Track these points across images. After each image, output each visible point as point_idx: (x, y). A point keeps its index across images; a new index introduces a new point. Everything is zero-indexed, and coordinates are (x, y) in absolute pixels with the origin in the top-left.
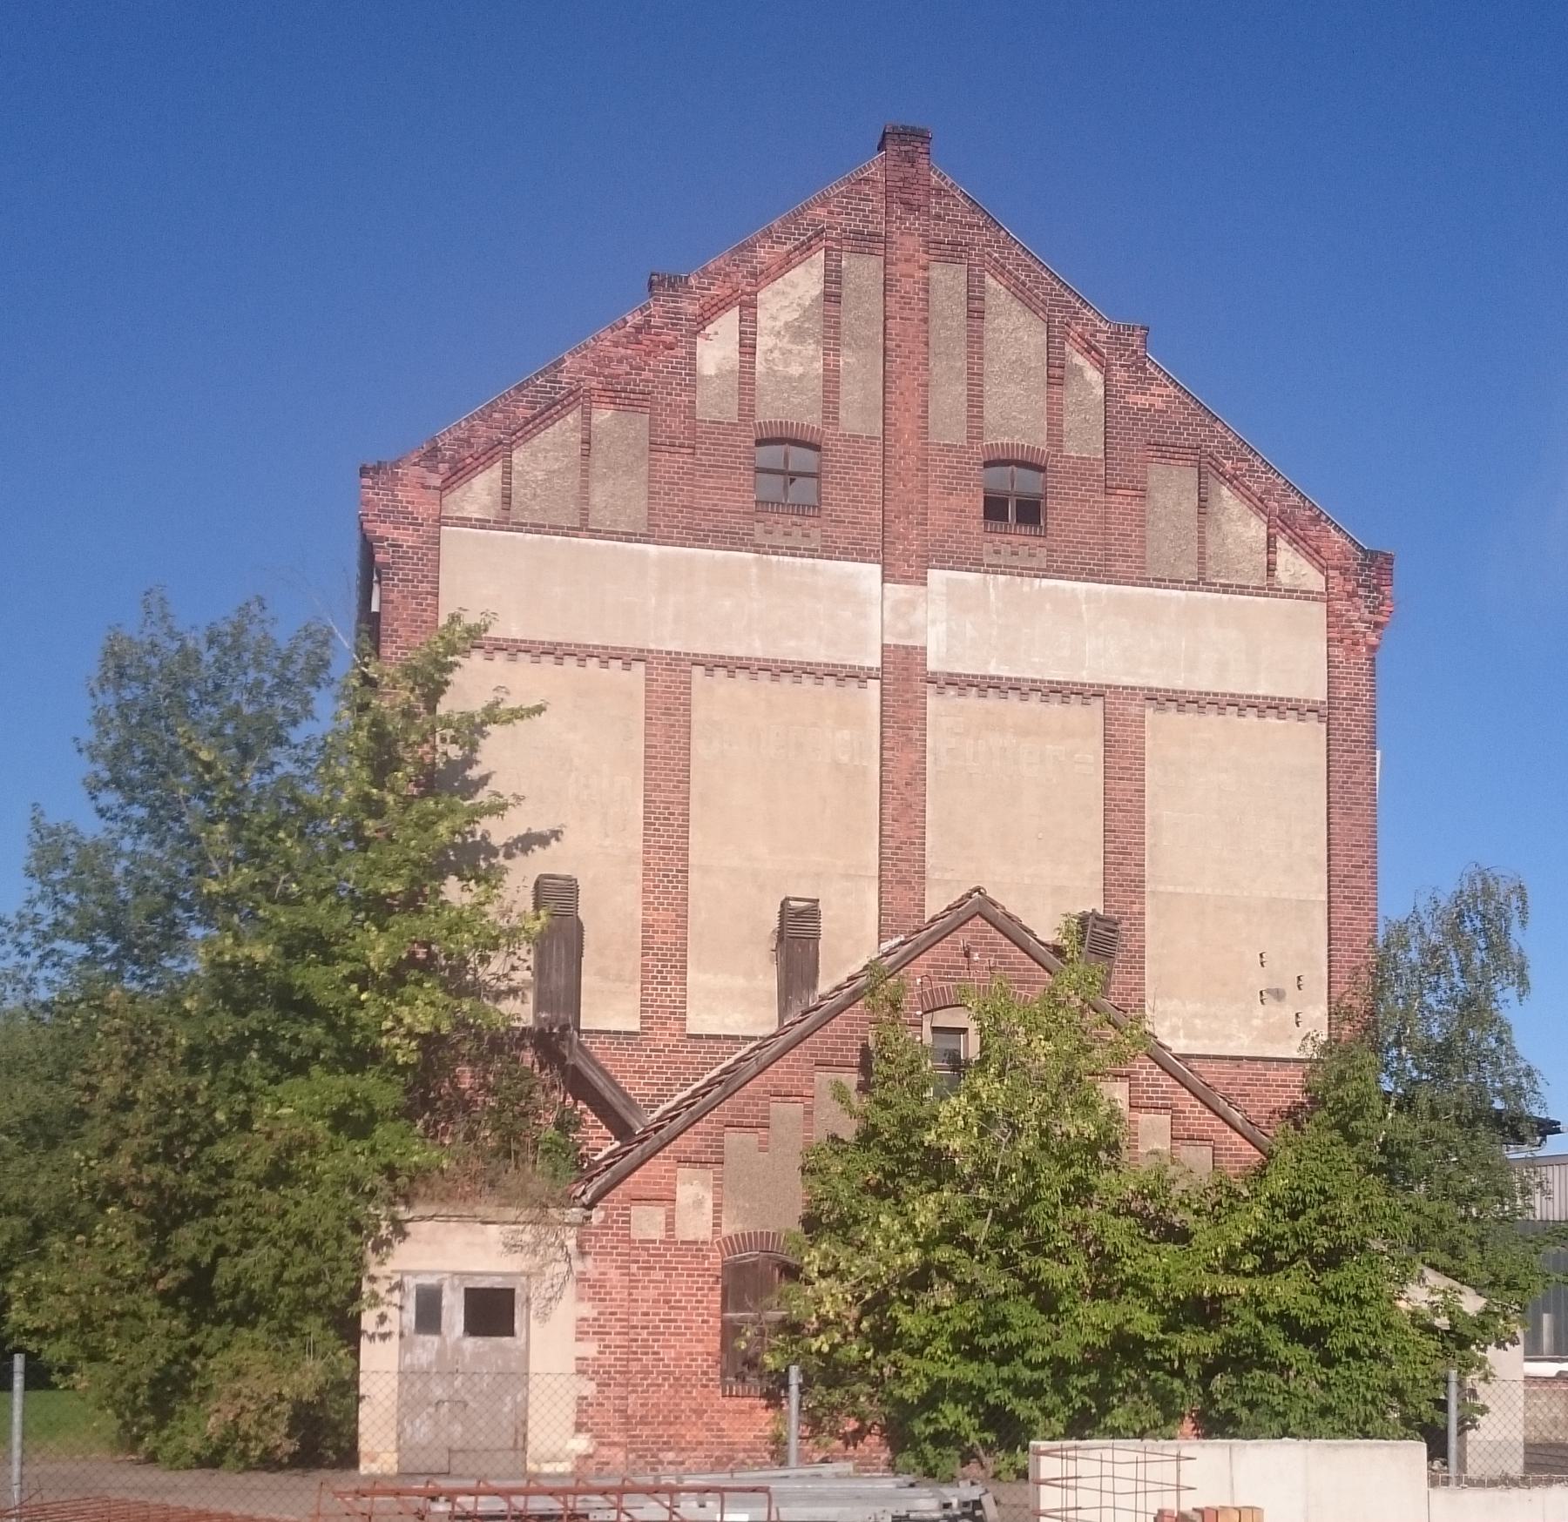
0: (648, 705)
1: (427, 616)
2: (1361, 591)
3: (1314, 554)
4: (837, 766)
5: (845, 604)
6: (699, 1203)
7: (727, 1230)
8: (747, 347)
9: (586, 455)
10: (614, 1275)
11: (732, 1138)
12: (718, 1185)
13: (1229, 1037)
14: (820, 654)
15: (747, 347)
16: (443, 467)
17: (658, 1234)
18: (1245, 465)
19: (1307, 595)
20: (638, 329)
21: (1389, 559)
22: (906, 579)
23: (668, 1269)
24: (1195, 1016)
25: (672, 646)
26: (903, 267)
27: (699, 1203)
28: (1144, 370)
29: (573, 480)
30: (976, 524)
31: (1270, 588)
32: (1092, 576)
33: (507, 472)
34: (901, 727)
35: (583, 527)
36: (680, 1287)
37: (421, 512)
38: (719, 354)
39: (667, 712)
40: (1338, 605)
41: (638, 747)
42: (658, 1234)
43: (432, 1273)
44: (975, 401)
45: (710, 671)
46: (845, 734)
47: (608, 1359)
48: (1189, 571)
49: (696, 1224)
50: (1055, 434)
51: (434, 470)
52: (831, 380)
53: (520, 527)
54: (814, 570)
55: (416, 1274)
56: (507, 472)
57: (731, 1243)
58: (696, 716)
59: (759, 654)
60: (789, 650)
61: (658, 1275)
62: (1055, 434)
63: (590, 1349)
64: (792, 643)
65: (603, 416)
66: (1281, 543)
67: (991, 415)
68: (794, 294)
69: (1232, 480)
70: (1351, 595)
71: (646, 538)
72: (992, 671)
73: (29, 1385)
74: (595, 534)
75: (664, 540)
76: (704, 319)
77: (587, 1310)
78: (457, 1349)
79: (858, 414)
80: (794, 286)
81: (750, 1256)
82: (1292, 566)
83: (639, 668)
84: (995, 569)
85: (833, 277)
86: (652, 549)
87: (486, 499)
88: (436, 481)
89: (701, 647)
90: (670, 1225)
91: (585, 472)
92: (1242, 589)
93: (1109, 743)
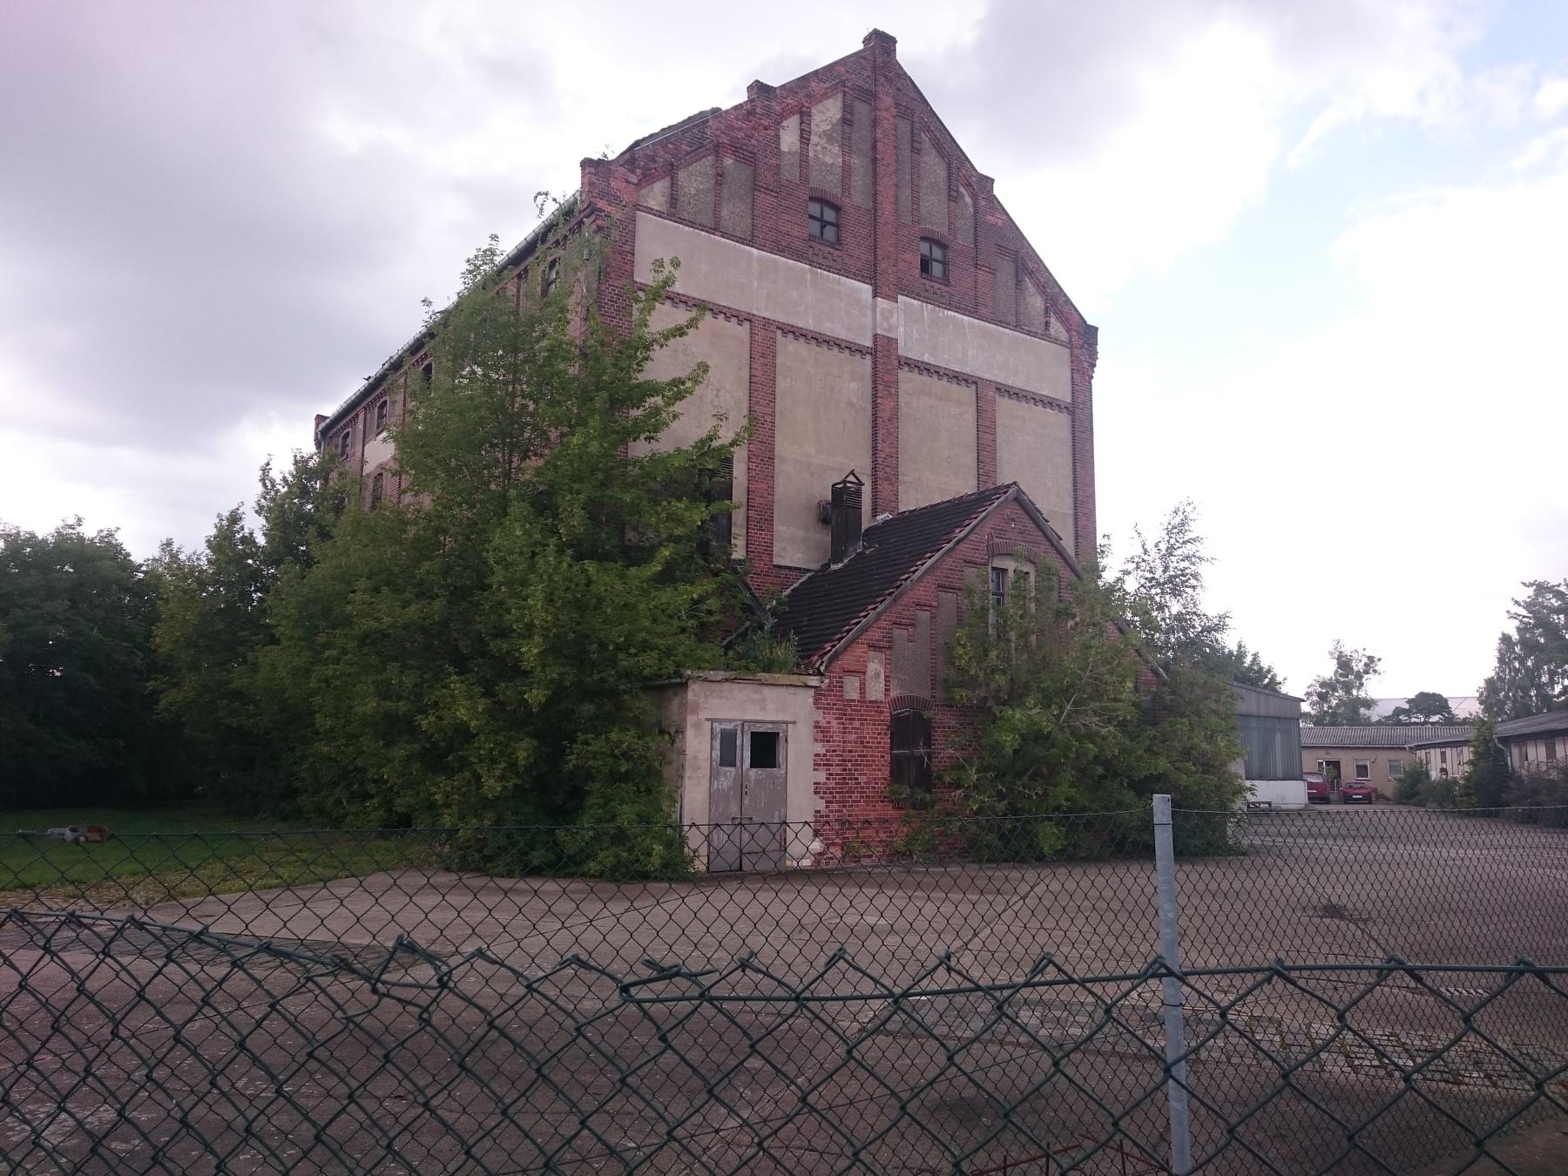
1: (627, 267)
6: (877, 675)
7: (894, 693)
9: (718, 184)
10: (834, 723)
11: (898, 632)
12: (888, 662)
14: (842, 334)
15: (805, 138)
16: (638, 171)
22: (887, 297)
25: (765, 315)
31: (1046, 336)
34: (882, 387)
35: (715, 229)
37: (626, 198)
39: (763, 356)
42: (855, 695)
43: (731, 721)
47: (832, 784)
49: (876, 691)
51: (633, 172)
52: (846, 170)
53: (681, 221)
54: (839, 282)
55: (720, 721)
56: (673, 184)
57: (896, 703)
58: (779, 360)
61: (857, 724)
63: (821, 776)
73: (1182, 853)
77: (820, 748)
79: (858, 197)
81: (905, 711)
85: (847, 109)
87: (662, 199)
89: (781, 318)
91: (718, 195)
93: (979, 411)
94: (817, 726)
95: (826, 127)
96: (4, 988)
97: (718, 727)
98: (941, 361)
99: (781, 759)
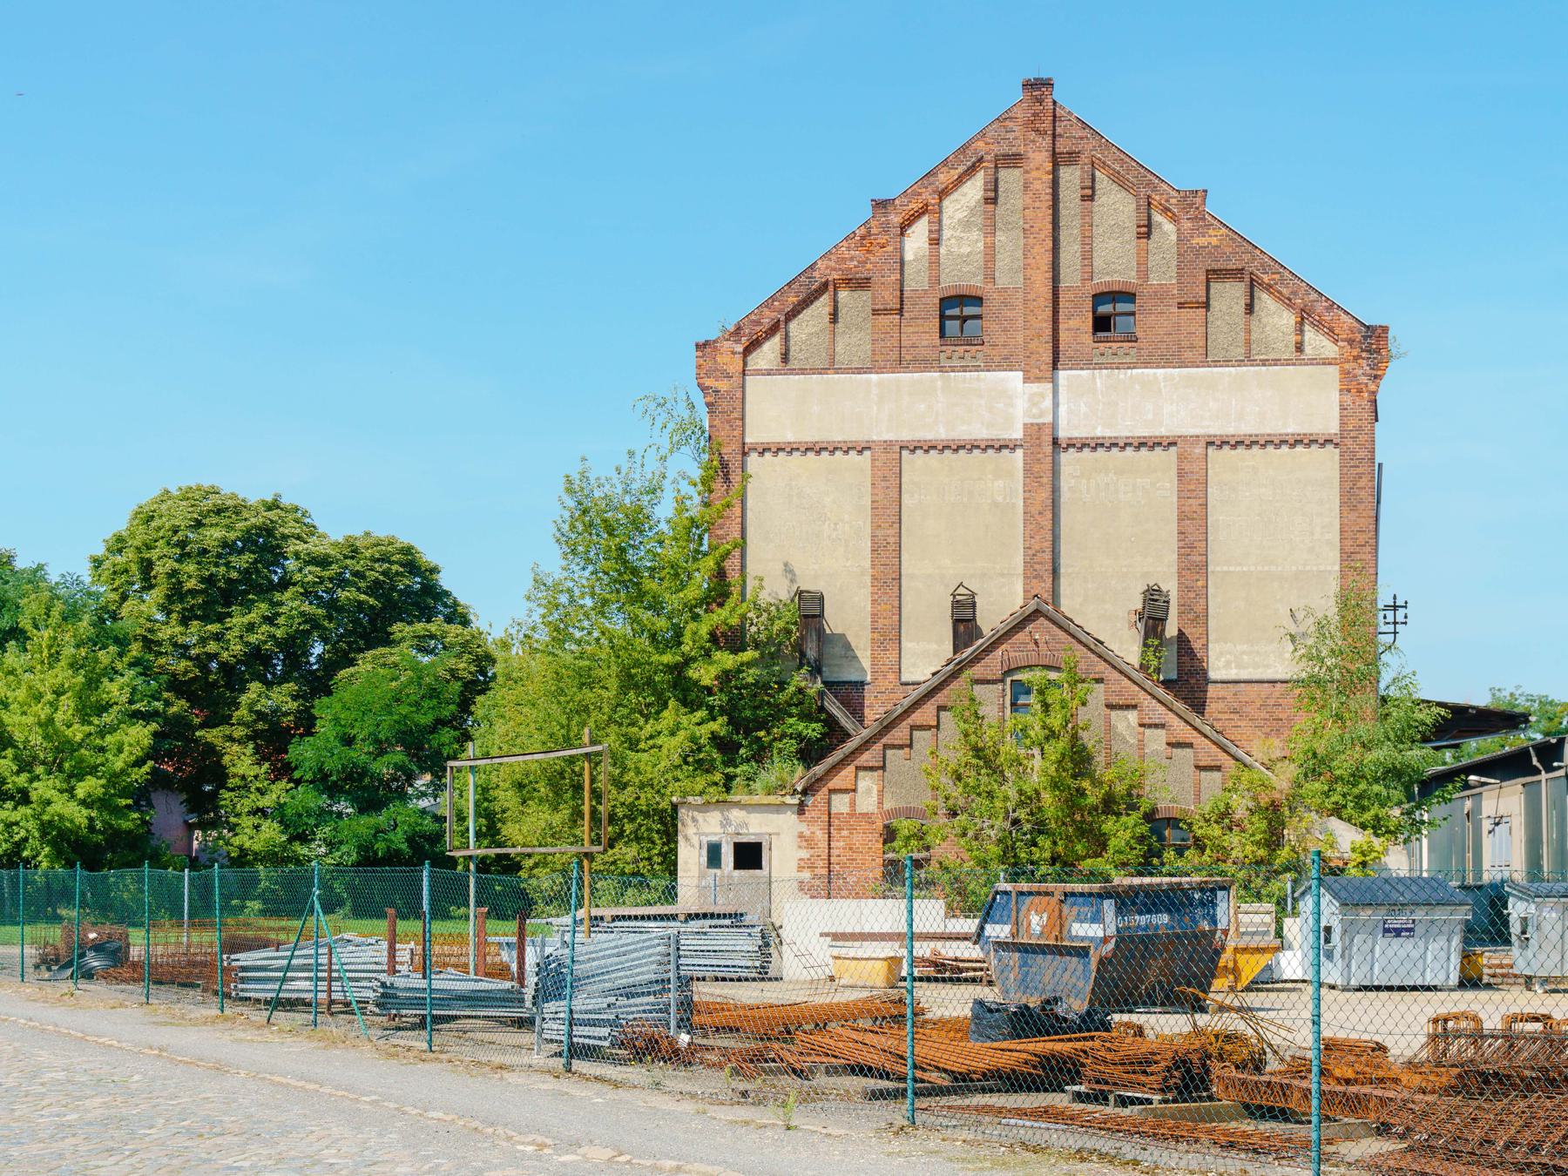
0: (873, 476)
3: (1331, 333)
4: (995, 504)
5: (1003, 399)
6: (869, 791)
7: (888, 806)
8: (935, 241)
13: (1268, 666)
14: (981, 433)
15: (935, 241)
17: (845, 809)
18: (1277, 277)
19: (1327, 362)
20: (863, 238)
21: (1385, 329)
23: (852, 830)
24: (1243, 653)
26: (1034, 174)
27: (869, 791)
28: (1204, 219)
29: (827, 337)
30: (1087, 338)
32: (1168, 364)
33: (787, 338)
36: (858, 839)
38: (916, 245)
40: (1347, 366)
41: (867, 501)
44: (1087, 256)
45: (913, 451)
46: (1000, 483)
48: (1239, 352)
50: (1144, 273)
52: (990, 253)
54: (978, 379)
59: (943, 437)
60: (965, 432)
62: (1144, 273)
63: (806, 875)
65: (843, 295)
66: (1307, 327)
67: (1098, 263)
69: (1268, 288)
70: (1356, 358)
71: (868, 371)
72: (1099, 434)
74: (838, 371)
75: (880, 370)
76: (903, 228)
77: (805, 854)
80: (965, 195)
82: (1315, 341)
83: (867, 453)
84: (1100, 366)
86: (874, 377)
88: (740, 348)
89: (906, 435)
90: (853, 804)
92: (1276, 362)
94: (801, 836)
95: (959, 215)
96: (28, 692)
97: (705, 840)
98: (1123, 430)
99: (764, 863)
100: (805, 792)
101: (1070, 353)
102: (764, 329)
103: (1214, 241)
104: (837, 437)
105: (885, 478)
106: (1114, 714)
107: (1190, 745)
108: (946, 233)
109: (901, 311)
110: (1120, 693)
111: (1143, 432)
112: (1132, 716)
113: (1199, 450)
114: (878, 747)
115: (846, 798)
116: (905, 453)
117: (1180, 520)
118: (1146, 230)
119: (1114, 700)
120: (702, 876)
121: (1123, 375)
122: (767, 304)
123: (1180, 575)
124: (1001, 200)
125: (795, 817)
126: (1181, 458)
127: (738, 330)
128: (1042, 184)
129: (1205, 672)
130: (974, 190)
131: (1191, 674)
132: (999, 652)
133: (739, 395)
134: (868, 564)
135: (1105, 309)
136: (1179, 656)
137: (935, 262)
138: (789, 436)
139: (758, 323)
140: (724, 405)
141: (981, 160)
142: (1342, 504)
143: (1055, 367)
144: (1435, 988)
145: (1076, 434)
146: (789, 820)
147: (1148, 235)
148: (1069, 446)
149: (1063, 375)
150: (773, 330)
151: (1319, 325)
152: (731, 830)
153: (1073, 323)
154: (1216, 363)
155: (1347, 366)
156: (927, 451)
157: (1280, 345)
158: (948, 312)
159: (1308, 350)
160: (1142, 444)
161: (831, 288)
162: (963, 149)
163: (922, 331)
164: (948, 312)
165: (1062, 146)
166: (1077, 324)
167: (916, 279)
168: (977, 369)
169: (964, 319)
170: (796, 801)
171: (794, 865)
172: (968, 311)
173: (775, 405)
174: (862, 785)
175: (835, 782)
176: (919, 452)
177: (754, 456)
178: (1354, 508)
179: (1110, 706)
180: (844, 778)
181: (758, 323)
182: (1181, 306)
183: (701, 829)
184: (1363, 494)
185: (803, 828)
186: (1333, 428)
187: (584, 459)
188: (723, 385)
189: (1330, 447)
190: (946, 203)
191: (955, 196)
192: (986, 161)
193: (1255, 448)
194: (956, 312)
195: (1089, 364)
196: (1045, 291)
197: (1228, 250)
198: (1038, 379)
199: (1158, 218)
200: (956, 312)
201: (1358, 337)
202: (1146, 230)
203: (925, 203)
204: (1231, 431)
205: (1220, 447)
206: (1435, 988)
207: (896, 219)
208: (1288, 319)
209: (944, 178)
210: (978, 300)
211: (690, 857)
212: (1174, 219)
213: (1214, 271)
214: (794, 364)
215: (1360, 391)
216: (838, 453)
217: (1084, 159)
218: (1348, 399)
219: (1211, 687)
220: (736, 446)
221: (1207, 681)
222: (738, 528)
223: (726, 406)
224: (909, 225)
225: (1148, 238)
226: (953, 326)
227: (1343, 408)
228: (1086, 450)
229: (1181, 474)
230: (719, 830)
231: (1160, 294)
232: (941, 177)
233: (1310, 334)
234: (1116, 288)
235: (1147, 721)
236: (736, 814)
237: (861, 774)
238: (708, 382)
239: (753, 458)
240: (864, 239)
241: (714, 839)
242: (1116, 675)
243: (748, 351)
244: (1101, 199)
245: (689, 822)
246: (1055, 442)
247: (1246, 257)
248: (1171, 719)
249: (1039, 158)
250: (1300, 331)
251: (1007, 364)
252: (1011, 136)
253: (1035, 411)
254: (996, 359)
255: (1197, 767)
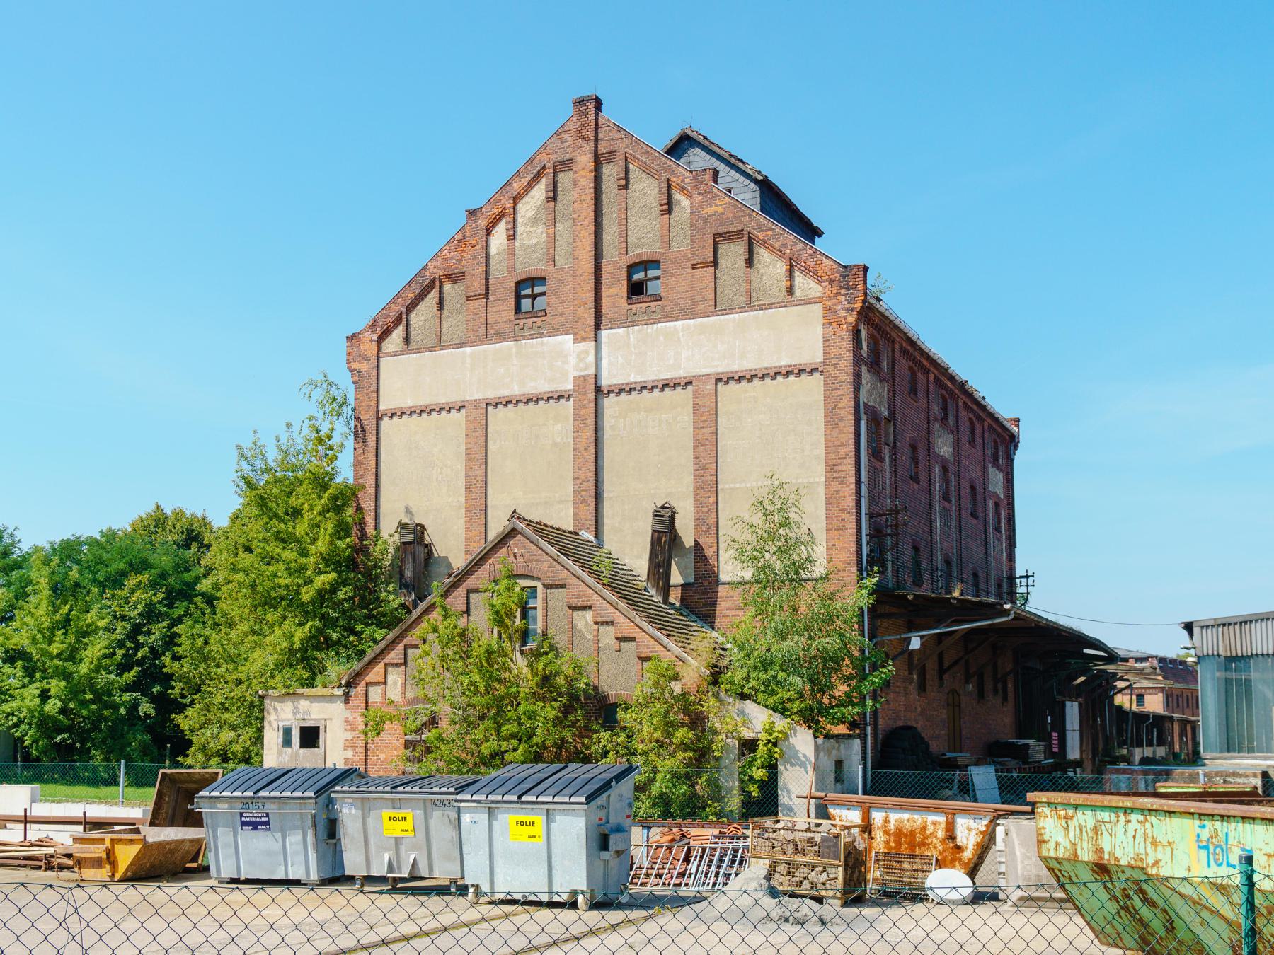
2: (843, 291)
4: (555, 444)
5: (559, 358)
6: (395, 683)
7: (409, 695)
8: (512, 237)
14: (543, 387)
15: (512, 237)
18: (770, 233)
19: (812, 302)
20: (460, 241)
25: (476, 397)
27: (395, 683)
30: (623, 301)
38: (498, 242)
40: (828, 303)
41: (463, 448)
44: (624, 234)
46: (558, 427)
48: (741, 300)
52: (552, 241)
54: (542, 344)
64: (533, 384)
66: (797, 273)
68: (533, 201)
69: (764, 243)
70: (836, 295)
73: (23, 761)
74: (443, 348)
76: (488, 232)
77: (349, 735)
78: (297, 754)
82: (803, 283)
83: (463, 411)
86: (468, 349)
88: (375, 337)
89: (490, 394)
92: (771, 306)
94: (347, 721)
95: (529, 214)
97: (281, 724)
100: (349, 685)
101: (611, 315)
102: (392, 323)
103: (720, 209)
104: (442, 399)
105: (475, 430)
106: (575, 613)
107: (633, 639)
108: (520, 230)
109: (487, 295)
110: (578, 597)
111: (666, 375)
112: (589, 615)
113: (710, 387)
114: (400, 647)
115: (379, 689)
116: (490, 408)
117: (695, 447)
118: (668, 206)
119: (574, 602)
120: (280, 753)
121: (651, 329)
122: (393, 301)
123: (696, 494)
124: (559, 198)
125: (342, 705)
126: (696, 395)
127: (374, 324)
128: (587, 182)
129: (716, 576)
130: (539, 193)
131: (704, 577)
132: (487, 566)
133: (375, 373)
134: (463, 499)
135: (639, 276)
136: (696, 562)
137: (512, 253)
138: (410, 402)
139: (388, 316)
140: (364, 382)
141: (543, 168)
142: (826, 423)
143: (598, 325)
144: (297, 883)
145: (615, 382)
146: (339, 706)
147: (669, 211)
148: (609, 392)
149: (605, 334)
150: (398, 321)
151: (806, 270)
152: (299, 717)
153: (613, 291)
154: (724, 312)
155: (828, 303)
156: (505, 405)
157: (775, 291)
158: (523, 293)
159: (798, 292)
160: (665, 386)
161: (437, 284)
162: (531, 161)
163: (502, 308)
164: (523, 293)
165: (602, 148)
166: (615, 291)
167: (499, 269)
168: (542, 336)
169: (534, 297)
170: (341, 693)
171: (341, 744)
172: (538, 289)
173: (404, 378)
174: (390, 678)
175: (372, 676)
176: (500, 407)
177: (386, 419)
178: (836, 426)
179: (573, 608)
180: (376, 673)
181: (388, 316)
182: (694, 267)
183: (283, 715)
184: (843, 412)
185: (348, 714)
186: (818, 358)
187: (255, 432)
188: (364, 367)
189: (817, 375)
190: (520, 206)
191: (526, 199)
192: (548, 172)
193: (756, 381)
194: (528, 292)
195: (626, 323)
196: (589, 267)
197: (730, 216)
198: (584, 339)
199: (677, 196)
200: (528, 292)
201: (837, 277)
202: (668, 206)
203: (503, 212)
204: (735, 367)
205: (727, 382)
206: (297, 883)
207: (482, 223)
208: (780, 268)
209: (517, 186)
210: (542, 280)
211: (272, 737)
212: (689, 196)
213: (720, 234)
214: (413, 345)
215: (840, 324)
216: (443, 413)
217: (620, 156)
218: (830, 331)
219: (721, 588)
220: (372, 413)
221: (718, 582)
222: (373, 476)
223: (369, 383)
224: (493, 227)
225: (670, 213)
226: (526, 304)
227: (826, 340)
228: (623, 394)
229: (696, 408)
230: (291, 716)
231: (678, 261)
232: (515, 185)
233: (799, 279)
234: (645, 258)
235: (599, 619)
236: (303, 704)
237: (390, 669)
238: (354, 366)
239: (385, 422)
240: (460, 242)
241: (287, 723)
242: (575, 581)
243: (381, 339)
244: (634, 186)
245: (272, 711)
246: (598, 390)
247: (745, 220)
248: (621, 619)
249: (585, 160)
250: (791, 276)
251: (563, 330)
252: (565, 145)
253: (581, 365)
254: (556, 326)
255: (639, 658)
